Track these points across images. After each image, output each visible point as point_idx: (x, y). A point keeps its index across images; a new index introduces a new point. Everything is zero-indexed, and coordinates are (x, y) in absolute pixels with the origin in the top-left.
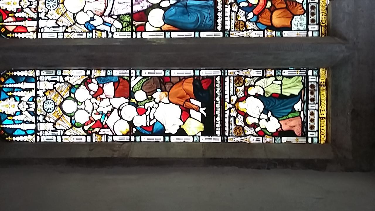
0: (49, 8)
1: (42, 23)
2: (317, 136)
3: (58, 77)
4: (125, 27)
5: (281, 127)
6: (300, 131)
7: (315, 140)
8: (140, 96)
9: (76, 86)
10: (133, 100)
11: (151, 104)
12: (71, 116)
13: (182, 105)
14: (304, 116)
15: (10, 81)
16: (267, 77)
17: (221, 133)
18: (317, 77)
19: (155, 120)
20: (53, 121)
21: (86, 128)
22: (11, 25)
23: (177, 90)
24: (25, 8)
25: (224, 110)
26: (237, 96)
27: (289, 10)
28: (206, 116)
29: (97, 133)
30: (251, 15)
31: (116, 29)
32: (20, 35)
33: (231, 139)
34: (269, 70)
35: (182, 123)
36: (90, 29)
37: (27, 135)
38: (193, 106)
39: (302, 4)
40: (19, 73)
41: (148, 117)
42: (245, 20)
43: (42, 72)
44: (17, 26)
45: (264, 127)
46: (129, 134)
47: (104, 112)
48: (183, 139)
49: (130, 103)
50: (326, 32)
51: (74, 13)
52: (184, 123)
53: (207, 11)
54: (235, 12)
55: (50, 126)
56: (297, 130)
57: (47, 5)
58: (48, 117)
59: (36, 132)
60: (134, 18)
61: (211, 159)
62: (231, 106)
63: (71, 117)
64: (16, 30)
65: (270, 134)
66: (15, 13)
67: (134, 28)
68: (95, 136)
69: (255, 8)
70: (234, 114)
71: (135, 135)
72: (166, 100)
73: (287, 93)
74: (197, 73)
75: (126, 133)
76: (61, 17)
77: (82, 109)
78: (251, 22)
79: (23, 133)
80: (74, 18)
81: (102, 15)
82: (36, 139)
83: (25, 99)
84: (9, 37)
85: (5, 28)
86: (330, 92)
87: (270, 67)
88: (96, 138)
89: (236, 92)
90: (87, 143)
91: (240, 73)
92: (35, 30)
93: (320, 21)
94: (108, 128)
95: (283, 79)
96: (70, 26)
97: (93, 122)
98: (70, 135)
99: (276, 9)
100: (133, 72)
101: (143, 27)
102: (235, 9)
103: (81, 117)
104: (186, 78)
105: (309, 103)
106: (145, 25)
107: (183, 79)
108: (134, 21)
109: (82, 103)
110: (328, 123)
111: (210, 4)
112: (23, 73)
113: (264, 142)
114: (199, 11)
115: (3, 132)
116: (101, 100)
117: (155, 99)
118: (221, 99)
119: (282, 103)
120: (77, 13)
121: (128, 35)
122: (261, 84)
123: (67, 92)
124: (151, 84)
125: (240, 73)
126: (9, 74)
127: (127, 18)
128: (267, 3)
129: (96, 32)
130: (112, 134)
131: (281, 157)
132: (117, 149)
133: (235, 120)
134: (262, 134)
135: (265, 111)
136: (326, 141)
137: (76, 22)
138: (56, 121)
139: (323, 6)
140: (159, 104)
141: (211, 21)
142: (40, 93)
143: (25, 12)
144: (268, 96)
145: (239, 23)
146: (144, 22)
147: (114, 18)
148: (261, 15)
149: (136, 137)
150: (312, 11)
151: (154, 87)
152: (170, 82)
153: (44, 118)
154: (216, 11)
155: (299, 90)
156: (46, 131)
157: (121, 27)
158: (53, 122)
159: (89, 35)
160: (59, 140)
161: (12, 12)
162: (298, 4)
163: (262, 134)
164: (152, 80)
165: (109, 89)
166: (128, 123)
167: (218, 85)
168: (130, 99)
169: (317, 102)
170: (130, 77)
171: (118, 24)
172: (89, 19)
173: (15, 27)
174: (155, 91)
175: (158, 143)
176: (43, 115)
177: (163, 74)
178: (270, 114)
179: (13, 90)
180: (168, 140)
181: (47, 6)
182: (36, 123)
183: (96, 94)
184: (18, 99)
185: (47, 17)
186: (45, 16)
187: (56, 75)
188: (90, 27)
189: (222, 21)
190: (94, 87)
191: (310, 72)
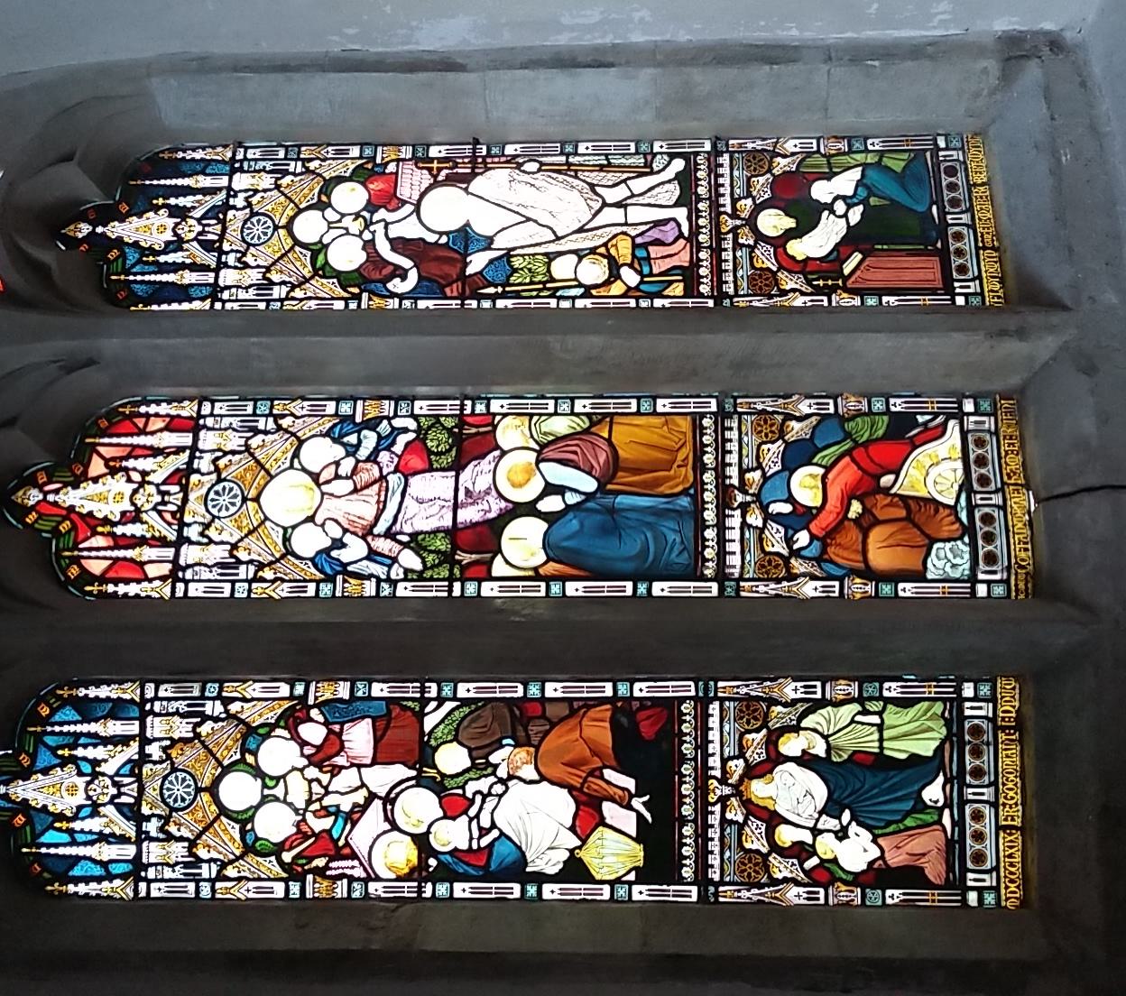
0: (215, 512)
1: (189, 554)
2: (994, 884)
3: (209, 704)
4: (433, 567)
5: (882, 857)
6: (942, 868)
7: (990, 899)
8: (452, 758)
9: (262, 731)
10: (432, 772)
11: (483, 785)
12: (244, 820)
13: (579, 785)
14: (954, 824)
15: (67, 715)
16: (838, 704)
17: (695, 873)
18: (991, 705)
19: (495, 833)
20: (185, 833)
21: (287, 857)
22: (97, 558)
23: (563, 740)
24: (146, 512)
25: (706, 803)
26: (746, 761)
27: (916, 526)
28: (650, 820)
29: (320, 872)
30: (803, 538)
31: (407, 571)
32: (122, 589)
33: (728, 894)
34: (843, 682)
35: (579, 843)
36: (328, 571)
37: (110, 877)
38: (612, 790)
39: (953, 509)
40: (92, 692)
41: (474, 823)
42: (785, 552)
43: (163, 687)
44: (116, 560)
45: (829, 856)
46: (416, 875)
47: (342, 808)
48: (579, 890)
49: (420, 781)
50: (1030, 585)
51: (286, 525)
52: (584, 842)
53: (672, 524)
54: (757, 527)
55: (178, 851)
56: (934, 869)
57: (210, 504)
58: (176, 824)
59: (137, 868)
60: (459, 543)
61: (669, 956)
62: (727, 791)
63: (243, 823)
64: (111, 575)
65: (850, 878)
66: (114, 524)
67: (457, 572)
68: (315, 882)
69: (815, 517)
70: (735, 814)
71: (435, 878)
72: (529, 772)
73: (899, 750)
74: (623, 689)
75: (406, 870)
76: (246, 536)
77: (277, 799)
78: (804, 558)
79: (98, 871)
80: (286, 540)
81: (367, 533)
82: (136, 891)
83: (109, 768)
84: (90, 593)
85: (81, 566)
86: (1030, 751)
87: (846, 674)
88: (315, 889)
89: (741, 746)
90: (290, 902)
91: (755, 689)
92: (167, 572)
93: (1013, 561)
94: (354, 856)
95: (884, 708)
96: (271, 563)
97: (310, 837)
98: (239, 879)
99: (878, 522)
100: (433, 690)
101: (484, 568)
102: (755, 519)
103: (274, 824)
104: (589, 704)
105: (968, 782)
106: (490, 563)
107: (580, 708)
108: (459, 552)
109: (278, 779)
110: (1029, 845)
111: (681, 506)
112: (104, 692)
113: (831, 902)
114: (648, 524)
115: (39, 869)
116: (336, 771)
117: (496, 766)
118: (695, 769)
119: (885, 781)
120: (294, 527)
121: (436, 591)
122: (818, 723)
123: (234, 750)
124: (483, 724)
125: (755, 689)
126: (65, 693)
127: (439, 543)
128: (849, 505)
129: (345, 581)
130: (363, 875)
131: (885, 953)
132: (378, 924)
133: (740, 835)
134: (825, 877)
135: (833, 808)
136: (1024, 902)
137: (289, 552)
138: (199, 836)
139: (1019, 515)
140: (510, 784)
141: (685, 555)
142: (154, 750)
143: (146, 523)
144: (839, 760)
145: (770, 562)
146: (489, 555)
147: (400, 542)
148: (834, 539)
149: (438, 886)
150: (986, 529)
151: (493, 734)
152: (543, 716)
153: (163, 826)
154: (701, 525)
155: (936, 743)
156: (168, 865)
157: (418, 565)
158: (187, 839)
159: (326, 589)
160: (206, 891)
161: (106, 521)
162: (941, 509)
163: (825, 877)
164: (487, 712)
165: (360, 737)
166: (415, 843)
167: (687, 728)
168: (421, 767)
169: (992, 779)
170: (424, 701)
171: (410, 560)
172: (328, 543)
173: (109, 562)
174: (498, 745)
175: (500, 904)
176: (160, 817)
177: (520, 693)
178: (846, 816)
179: (75, 740)
180: (535, 895)
181: (210, 507)
182: (139, 843)
183: (321, 755)
184: (87, 768)
185: (208, 537)
186: (202, 534)
187: (203, 697)
188: (328, 564)
189: (718, 554)
190: (314, 732)
191: (968, 690)
